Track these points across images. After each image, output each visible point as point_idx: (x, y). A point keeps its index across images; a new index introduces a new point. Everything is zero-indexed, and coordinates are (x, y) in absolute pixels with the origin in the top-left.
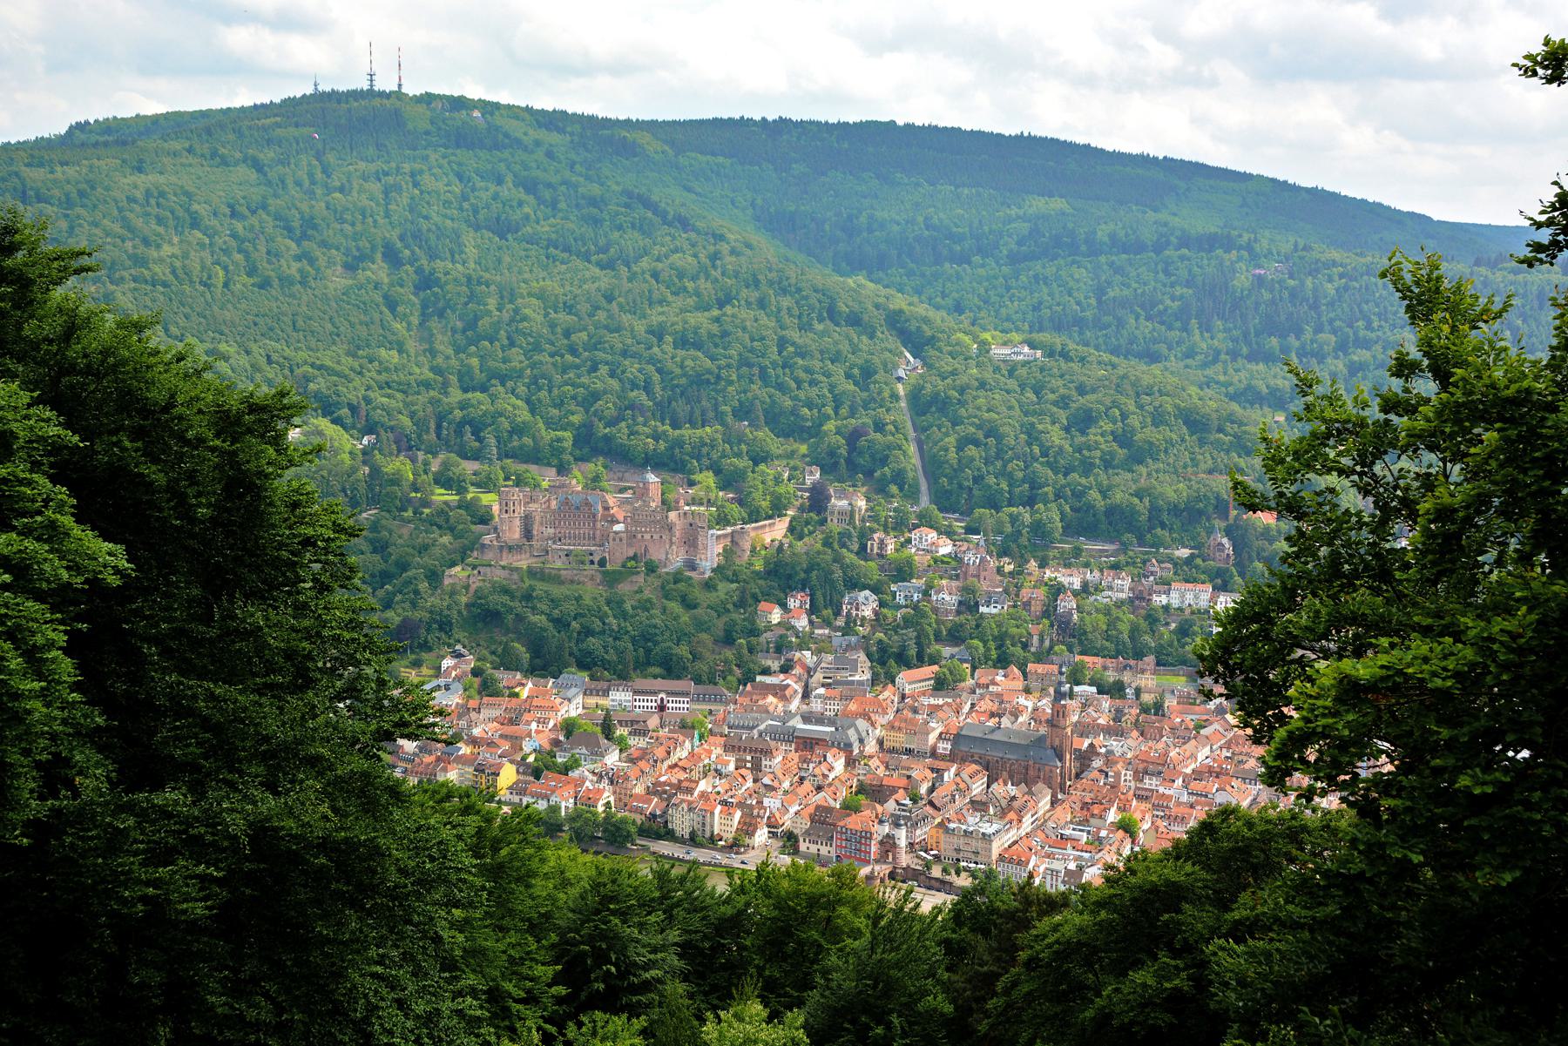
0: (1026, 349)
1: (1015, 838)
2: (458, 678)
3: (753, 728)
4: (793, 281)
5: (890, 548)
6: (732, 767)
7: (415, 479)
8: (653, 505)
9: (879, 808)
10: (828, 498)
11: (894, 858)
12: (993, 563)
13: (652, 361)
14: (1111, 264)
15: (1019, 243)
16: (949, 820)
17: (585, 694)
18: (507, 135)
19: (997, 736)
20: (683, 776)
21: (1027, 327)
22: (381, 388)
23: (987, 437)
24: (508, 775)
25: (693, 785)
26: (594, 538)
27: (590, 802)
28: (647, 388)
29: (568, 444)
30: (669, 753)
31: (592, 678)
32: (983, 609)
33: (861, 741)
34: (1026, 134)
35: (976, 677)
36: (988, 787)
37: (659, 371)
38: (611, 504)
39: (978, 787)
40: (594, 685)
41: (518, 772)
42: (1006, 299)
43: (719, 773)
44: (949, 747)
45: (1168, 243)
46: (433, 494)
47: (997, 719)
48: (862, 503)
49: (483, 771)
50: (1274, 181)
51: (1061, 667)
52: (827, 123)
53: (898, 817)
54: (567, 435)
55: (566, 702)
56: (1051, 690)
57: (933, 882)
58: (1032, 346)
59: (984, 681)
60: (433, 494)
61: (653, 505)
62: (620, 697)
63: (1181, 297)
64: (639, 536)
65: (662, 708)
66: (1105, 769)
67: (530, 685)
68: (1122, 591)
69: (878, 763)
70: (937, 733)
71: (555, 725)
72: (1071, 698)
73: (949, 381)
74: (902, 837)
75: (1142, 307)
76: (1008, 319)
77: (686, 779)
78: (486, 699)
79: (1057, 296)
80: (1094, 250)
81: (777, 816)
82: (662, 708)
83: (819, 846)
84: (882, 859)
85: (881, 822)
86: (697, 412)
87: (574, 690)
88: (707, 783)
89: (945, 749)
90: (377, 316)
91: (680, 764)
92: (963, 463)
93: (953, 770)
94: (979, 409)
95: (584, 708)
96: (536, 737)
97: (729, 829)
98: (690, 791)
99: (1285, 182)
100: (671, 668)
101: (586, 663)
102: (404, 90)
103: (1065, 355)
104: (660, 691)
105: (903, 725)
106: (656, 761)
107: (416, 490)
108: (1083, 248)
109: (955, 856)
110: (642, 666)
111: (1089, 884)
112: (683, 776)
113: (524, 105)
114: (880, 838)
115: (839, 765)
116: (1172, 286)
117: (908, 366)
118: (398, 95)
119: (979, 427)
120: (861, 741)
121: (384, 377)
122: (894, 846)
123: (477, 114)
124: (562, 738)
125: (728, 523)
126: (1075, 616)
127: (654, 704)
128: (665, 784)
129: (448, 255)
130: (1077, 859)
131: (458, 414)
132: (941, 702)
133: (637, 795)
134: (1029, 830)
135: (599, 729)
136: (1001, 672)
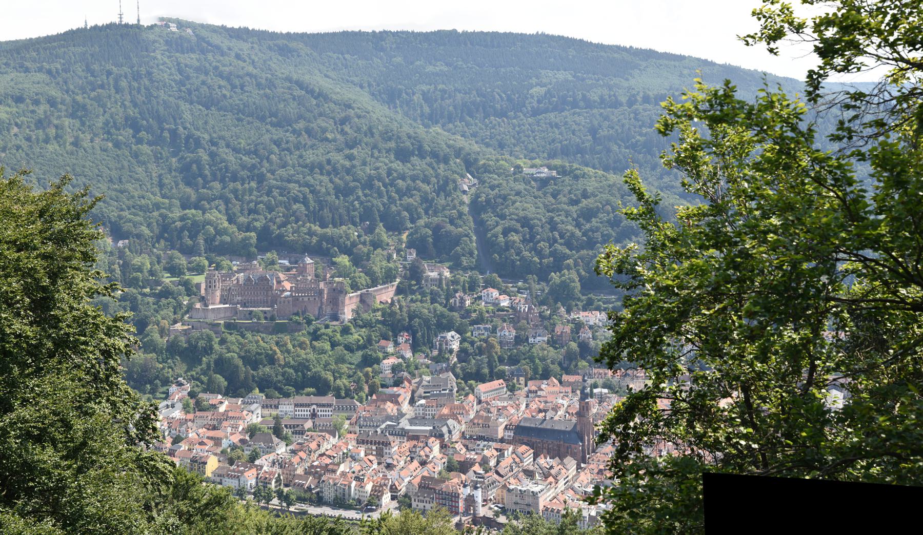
0: (546, 170)
2: (180, 400)
3: (377, 426)
4: (395, 132)
5: (468, 303)
6: (362, 454)
7: (151, 268)
8: (309, 278)
9: (463, 477)
10: (423, 271)
11: (474, 510)
12: (536, 310)
13: (307, 185)
14: (601, 114)
15: (539, 102)
17: (263, 407)
18: (209, 43)
19: (544, 426)
20: (328, 461)
21: (546, 155)
22: (129, 209)
23: (523, 227)
24: (212, 465)
25: (336, 467)
26: (267, 302)
27: (267, 481)
28: (305, 202)
29: (254, 241)
30: (319, 446)
31: (267, 397)
32: (531, 340)
33: (450, 432)
34: (540, 33)
36: (534, 460)
37: (311, 192)
38: (282, 279)
39: (528, 461)
40: (269, 401)
41: (219, 461)
42: (531, 138)
43: (354, 459)
45: (636, 101)
46: (163, 277)
47: (544, 414)
48: (447, 274)
49: (196, 461)
50: (699, 60)
51: (584, 377)
52: (413, 32)
53: (477, 482)
54: (253, 234)
55: (250, 414)
56: (578, 392)
58: (550, 168)
59: (534, 388)
60: (163, 277)
61: (309, 278)
62: (287, 408)
63: (645, 135)
64: (301, 299)
65: (314, 415)
67: (226, 403)
69: (462, 447)
70: (503, 426)
71: (243, 429)
72: (592, 397)
73: (497, 190)
74: (479, 495)
75: (622, 140)
76: (533, 151)
77: (331, 464)
78: (198, 413)
79: (565, 134)
80: (589, 105)
81: (397, 484)
82: (314, 415)
83: (425, 504)
84: (466, 513)
85: (465, 486)
86: (336, 217)
87: (255, 405)
88: (345, 466)
89: (509, 436)
90: (126, 164)
91: (327, 453)
92: (508, 245)
93: (511, 449)
94: (517, 209)
95: (262, 417)
96: (231, 436)
97: (365, 495)
98: (334, 471)
99: (706, 60)
100: (322, 388)
101: (265, 385)
102: (141, 23)
104: (312, 404)
105: (480, 422)
106: (310, 452)
107: (152, 275)
108: (582, 104)
110: (299, 387)
112: (328, 461)
113: (220, 25)
114: (464, 497)
115: (436, 448)
116: (640, 127)
117: (467, 183)
118: (138, 27)
119: (517, 221)
120: (450, 432)
121: (131, 203)
122: (474, 502)
123: (189, 31)
124: (248, 438)
125: (359, 289)
127: (308, 413)
128: (317, 467)
129: (172, 120)
131: (179, 224)
133: (299, 475)
134: (563, 488)
135: (271, 431)
136: (545, 382)
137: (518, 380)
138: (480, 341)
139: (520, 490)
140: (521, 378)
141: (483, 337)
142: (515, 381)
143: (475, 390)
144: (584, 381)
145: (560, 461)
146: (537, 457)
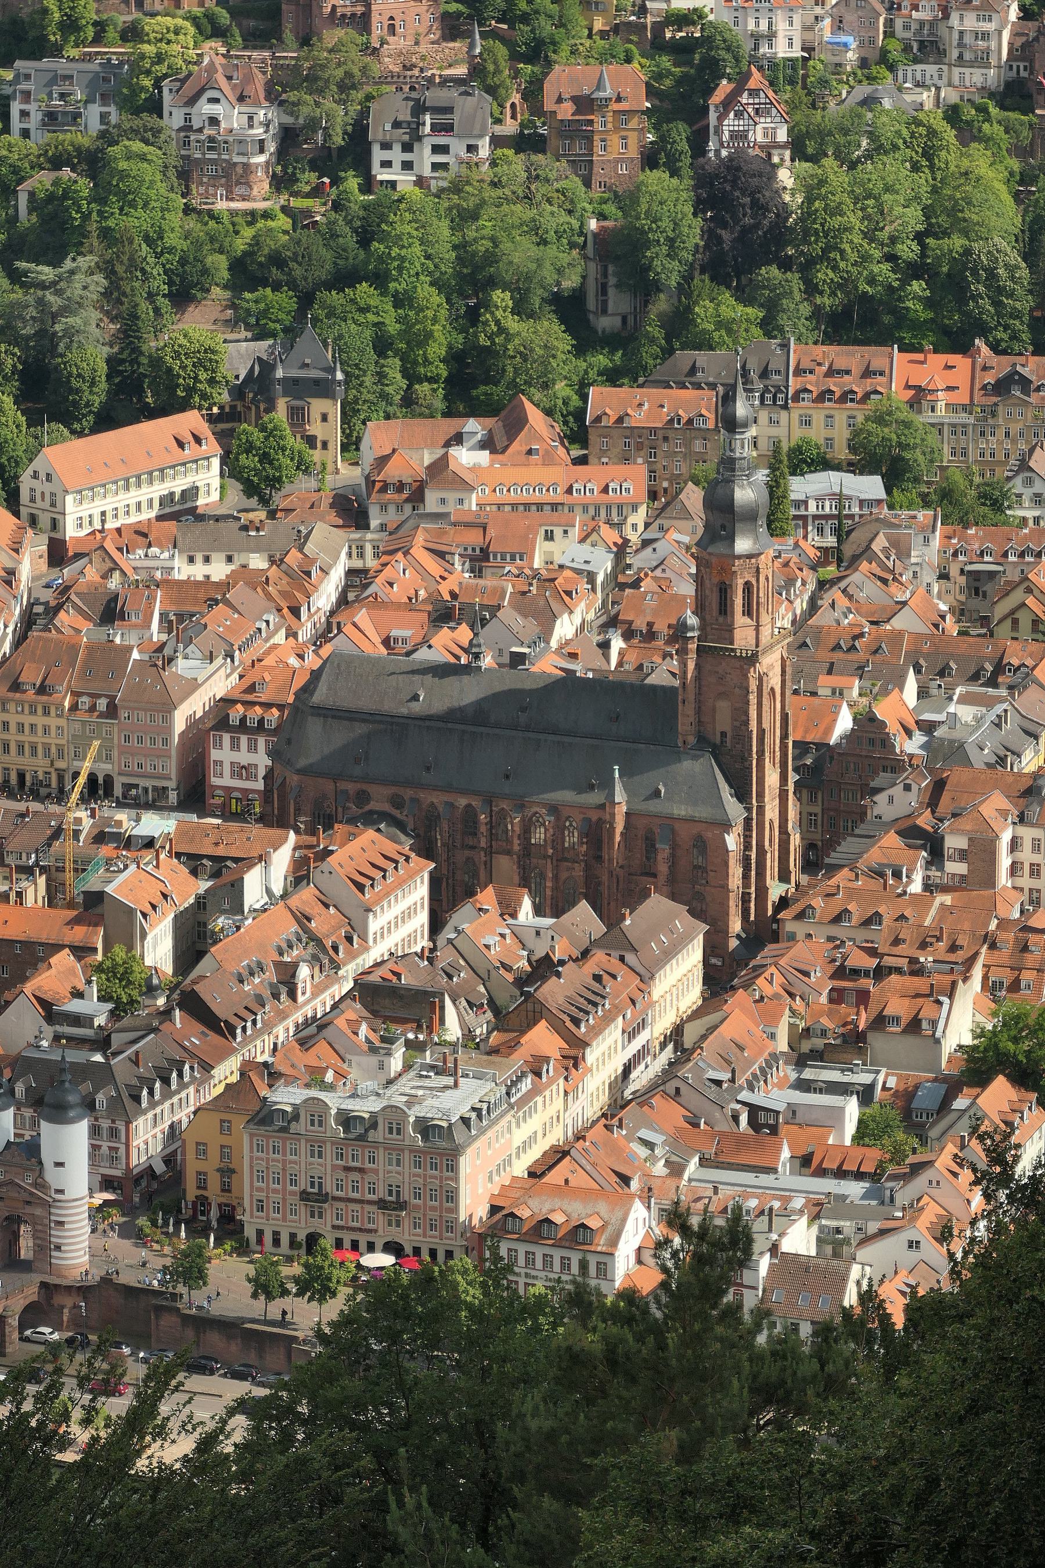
1: (556, 1136)
16: (272, 1075)
35: (368, 452)
36: (436, 925)
44: (262, 761)
47: (464, 634)
51: (728, 399)
56: (693, 497)
57: (214, 1339)
66: (925, 821)
68: (982, 60)
89: (243, 771)
93: (282, 859)
102: (845, 492)
103: (17, 427)
109: (302, 1225)
111: (629, 1295)
126: (785, 177)
130: (817, 1210)
132: (219, 570)
137: (298, 417)
138: (56, 163)
139: (347, 1120)
140: (318, 406)
141: (70, 138)
142: (281, 413)
143: (26, 483)
144: (731, 424)
145: (597, 927)
146: (454, 904)
